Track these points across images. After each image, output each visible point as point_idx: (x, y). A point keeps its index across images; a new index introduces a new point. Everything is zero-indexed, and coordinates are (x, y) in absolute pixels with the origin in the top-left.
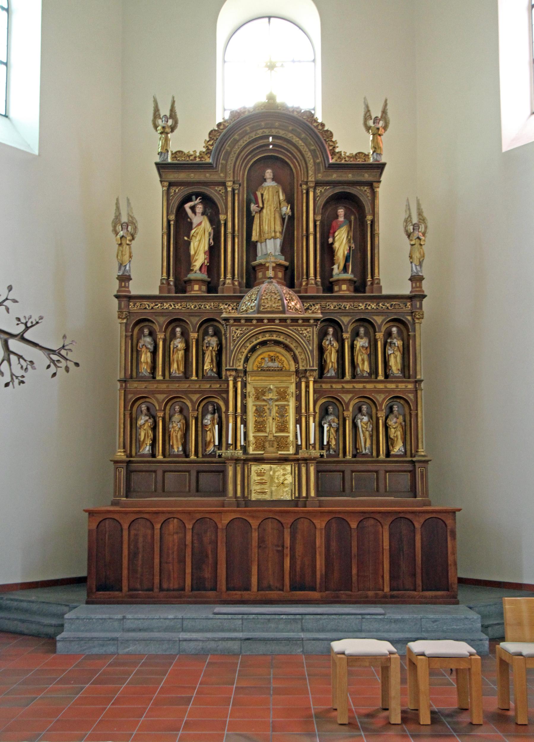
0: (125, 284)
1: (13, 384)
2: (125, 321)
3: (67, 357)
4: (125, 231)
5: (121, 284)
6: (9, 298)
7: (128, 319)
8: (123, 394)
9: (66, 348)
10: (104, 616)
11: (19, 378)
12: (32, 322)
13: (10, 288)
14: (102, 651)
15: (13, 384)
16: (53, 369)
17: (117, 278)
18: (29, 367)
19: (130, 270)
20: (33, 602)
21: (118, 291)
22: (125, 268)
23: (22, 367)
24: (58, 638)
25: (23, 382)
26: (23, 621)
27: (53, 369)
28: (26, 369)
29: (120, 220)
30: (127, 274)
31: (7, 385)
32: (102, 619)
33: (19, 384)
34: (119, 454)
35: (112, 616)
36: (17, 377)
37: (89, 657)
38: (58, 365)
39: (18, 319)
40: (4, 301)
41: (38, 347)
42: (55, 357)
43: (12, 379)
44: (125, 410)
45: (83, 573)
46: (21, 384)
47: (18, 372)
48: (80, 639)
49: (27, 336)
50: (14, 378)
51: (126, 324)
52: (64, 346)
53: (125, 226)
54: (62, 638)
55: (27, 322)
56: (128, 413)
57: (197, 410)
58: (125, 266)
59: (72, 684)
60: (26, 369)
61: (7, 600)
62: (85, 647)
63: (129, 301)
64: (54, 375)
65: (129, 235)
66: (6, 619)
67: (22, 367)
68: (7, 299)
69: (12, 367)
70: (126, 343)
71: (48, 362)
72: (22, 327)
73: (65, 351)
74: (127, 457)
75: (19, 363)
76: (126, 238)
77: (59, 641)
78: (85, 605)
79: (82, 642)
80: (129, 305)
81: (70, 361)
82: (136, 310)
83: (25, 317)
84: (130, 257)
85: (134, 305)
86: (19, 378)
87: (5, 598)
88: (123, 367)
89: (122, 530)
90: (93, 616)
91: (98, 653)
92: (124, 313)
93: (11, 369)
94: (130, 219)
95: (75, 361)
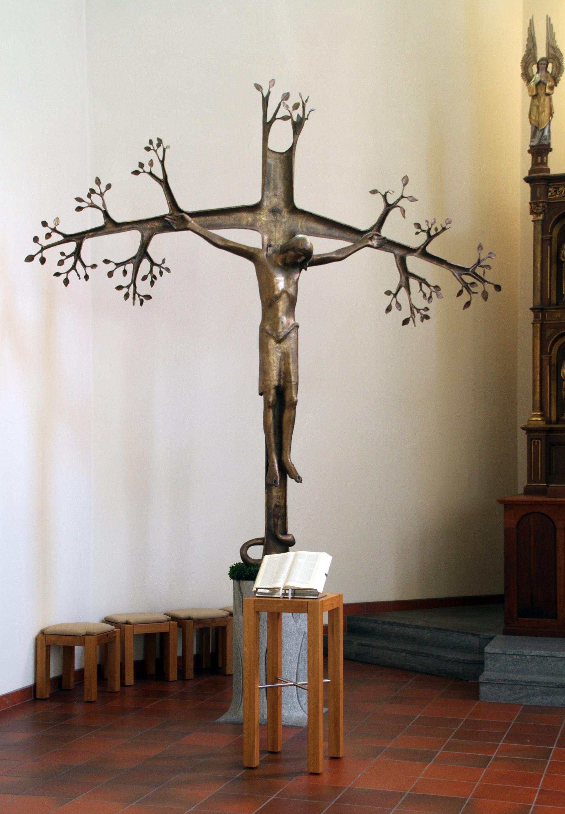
0: (542, 160)
1: (414, 321)
2: (541, 217)
3: (485, 278)
4: (544, 72)
5: (537, 159)
6: (404, 195)
7: (545, 214)
8: (538, 330)
9: (482, 264)
10: (543, 653)
11: (422, 311)
12: (436, 229)
13: (406, 180)
14: (547, 701)
15: (414, 321)
16: (466, 296)
17: (529, 151)
18: (434, 295)
19: (549, 136)
20: (423, 628)
21: (531, 172)
22: (543, 133)
23: (425, 295)
24: (481, 679)
25: (427, 317)
26: (415, 654)
27: (466, 296)
28: (431, 297)
29: (535, 56)
30: (546, 143)
31: (406, 322)
32: (539, 656)
33: (422, 321)
34: (534, 419)
35: (554, 653)
36: (418, 310)
37: (529, 709)
38: (473, 289)
39: (418, 226)
40: (399, 200)
41: (444, 266)
42: (468, 279)
43: (412, 313)
44: (541, 353)
45: (498, 589)
46: (425, 320)
47: (420, 303)
48: (514, 683)
49: (430, 249)
50: (415, 311)
51: (543, 221)
52: (479, 262)
53: (542, 65)
54: (487, 680)
55: (429, 229)
56: (545, 357)
57: (550, 353)
58: (543, 130)
59: (528, 743)
60: (431, 297)
61: (384, 623)
62: (521, 695)
63: (548, 186)
64: (468, 304)
65: (550, 78)
66: (389, 649)
67: (425, 295)
68: (402, 197)
69: (411, 296)
70: (542, 252)
71: (459, 286)
72: (423, 237)
73: (482, 269)
74: (547, 423)
75: (421, 290)
76: (545, 84)
77: (482, 683)
78: (502, 636)
79: (516, 687)
80: (548, 191)
81: (488, 283)
82: (559, 198)
83: (427, 221)
84: (551, 114)
85: (556, 191)
86: (422, 311)
87: (380, 622)
88: (539, 288)
89: (555, 529)
90: (526, 652)
91: (541, 704)
92: (541, 205)
93: (410, 300)
94: (552, 51)
95: (496, 283)
